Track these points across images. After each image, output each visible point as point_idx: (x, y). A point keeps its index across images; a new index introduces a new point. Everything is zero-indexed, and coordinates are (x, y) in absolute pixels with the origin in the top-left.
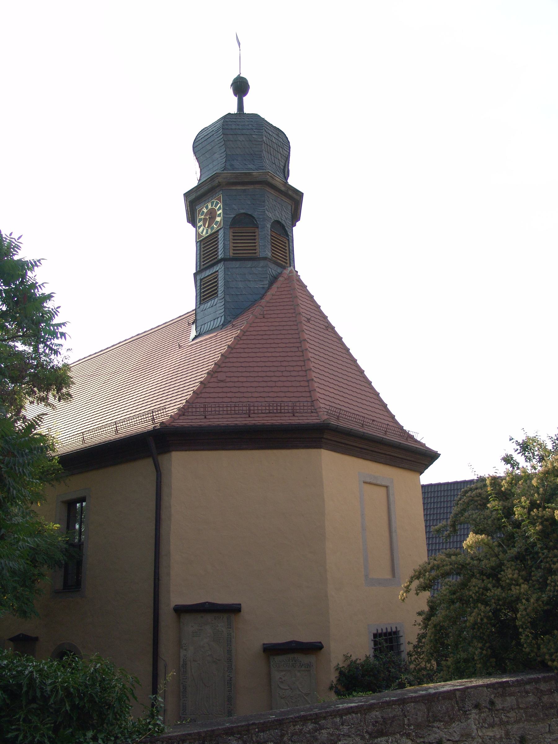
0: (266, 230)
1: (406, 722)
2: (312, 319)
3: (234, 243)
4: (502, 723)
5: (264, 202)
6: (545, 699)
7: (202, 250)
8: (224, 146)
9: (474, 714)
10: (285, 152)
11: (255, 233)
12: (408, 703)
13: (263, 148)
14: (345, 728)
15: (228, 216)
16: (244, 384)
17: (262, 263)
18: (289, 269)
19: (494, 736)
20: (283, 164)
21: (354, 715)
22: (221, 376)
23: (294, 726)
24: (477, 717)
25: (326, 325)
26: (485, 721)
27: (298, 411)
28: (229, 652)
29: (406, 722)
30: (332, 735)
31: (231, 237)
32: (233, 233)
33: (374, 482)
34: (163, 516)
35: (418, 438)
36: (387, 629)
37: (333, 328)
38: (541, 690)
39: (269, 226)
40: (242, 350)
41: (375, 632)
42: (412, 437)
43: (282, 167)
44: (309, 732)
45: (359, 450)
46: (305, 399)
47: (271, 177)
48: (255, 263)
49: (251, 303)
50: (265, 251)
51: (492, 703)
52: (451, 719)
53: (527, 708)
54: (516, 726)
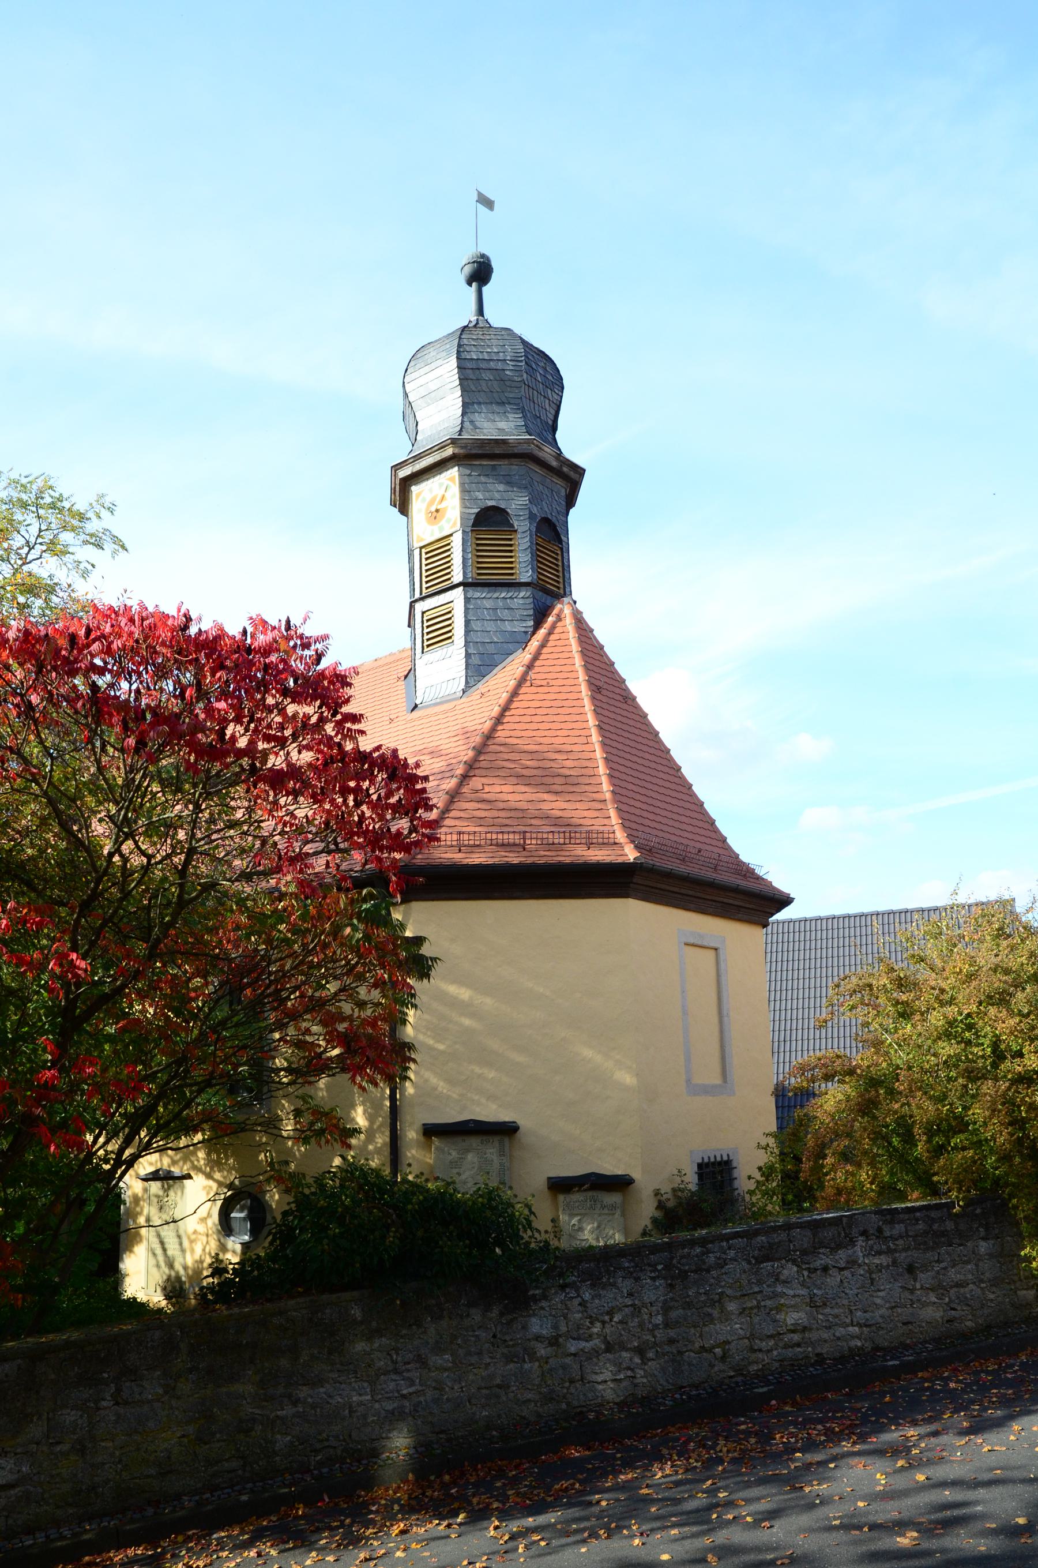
4: (889, 1251)
9: (860, 1242)
10: (555, 396)
14: (732, 1253)
30: (719, 1258)
31: (474, 546)
33: (699, 943)
35: (760, 872)
41: (700, 1161)
42: (752, 872)
43: (550, 422)
44: (697, 1256)
51: (880, 1230)
53: (916, 1236)
54: (904, 1254)
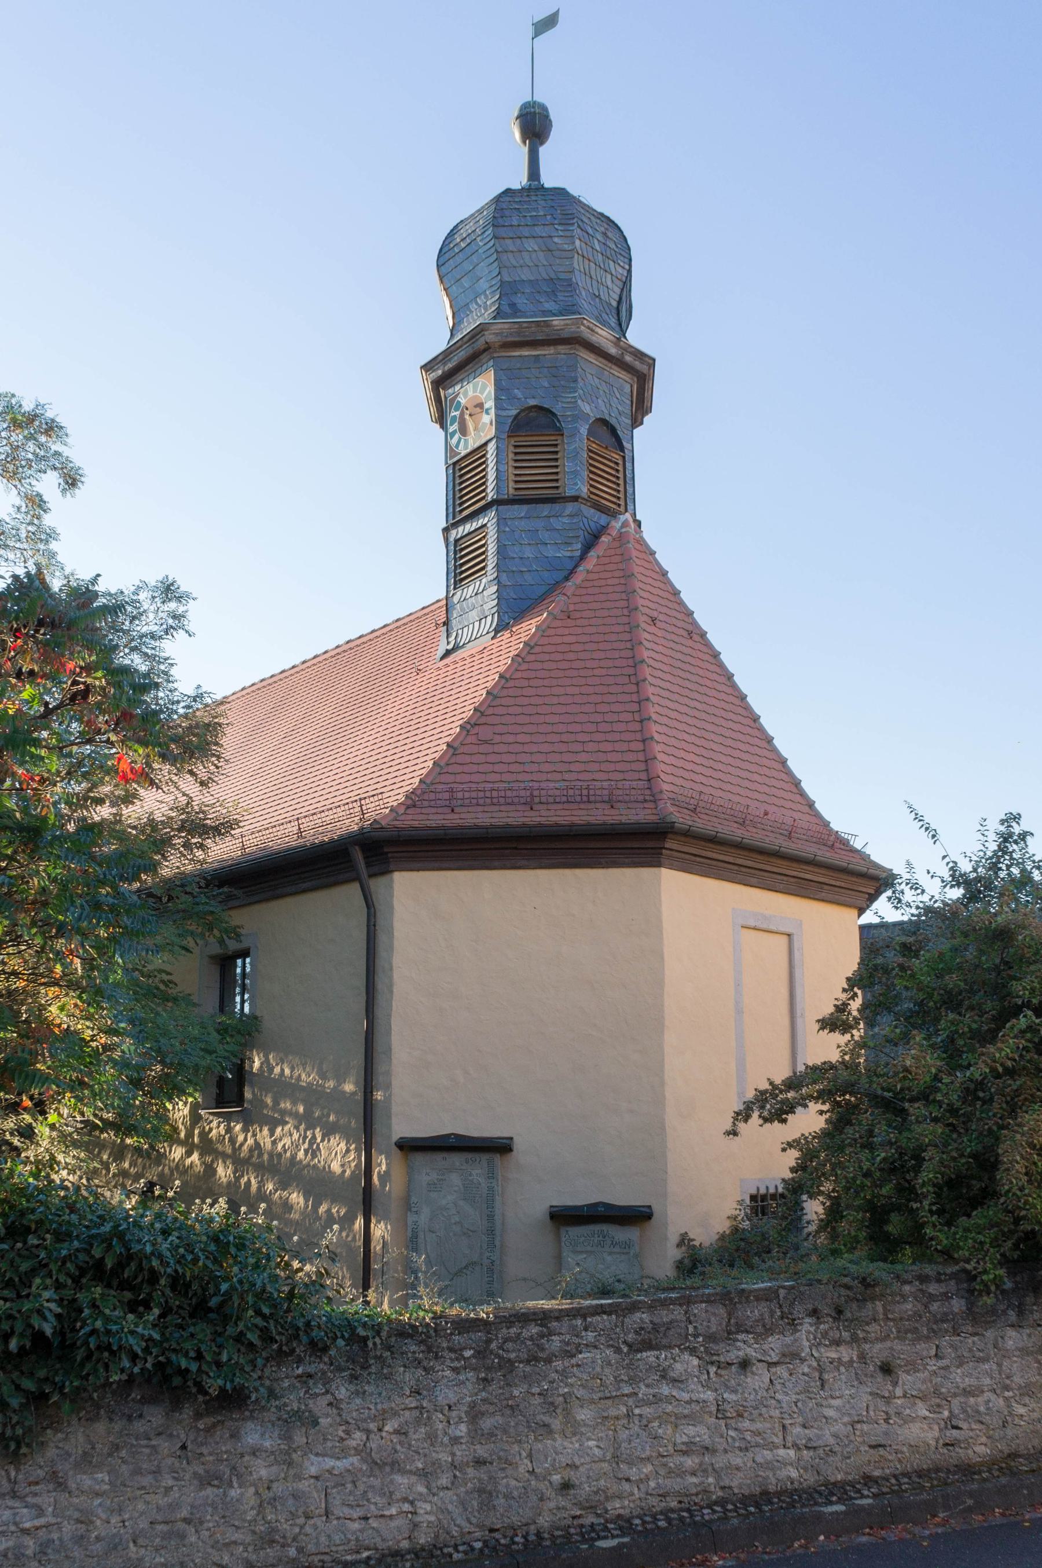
0: (578, 442)
1: (691, 1330)
2: (661, 617)
3: (516, 468)
5: (575, 381)
6: (935, 1307)
7: (458, 481)
8: (496, 264)
10: (620, 270)
11: (556, 445)
12: (696, 1302)
13: (576, 265)
14: (590, 1336)
15: (504, 413)
16: (526, 748)
17: (570, 508)
18: (622, 518)
19: (839, 1359)
20: (617, 298)
21: (605, 1317)
22: (485, 733)
23: (508, 1328)
24: (812, 1329)
25: (690, 628)
26: (825, 1334)
27: (620, 798)
28: (491, 1217)
29: (691, 1330)
30: (568, 1344)
31: (511, 456)
32: (516, 446)
33: (764, 926)
34: (380, 985)
36: (767, 1188)
37: (703, 635)
38: (930, 1294)
39: (584, 430)
40: (525, 683)
41: (754, 1192)
42: (845, 843)
43: (614, 304)
44: (531, 1338)
45: (736, 868)
46: (636, 776)
47: (589, 328)
48: (557, 507)
49: (548, 587)
50: (576, 484)
52: (767, 1330)
53: (901, 1319)
